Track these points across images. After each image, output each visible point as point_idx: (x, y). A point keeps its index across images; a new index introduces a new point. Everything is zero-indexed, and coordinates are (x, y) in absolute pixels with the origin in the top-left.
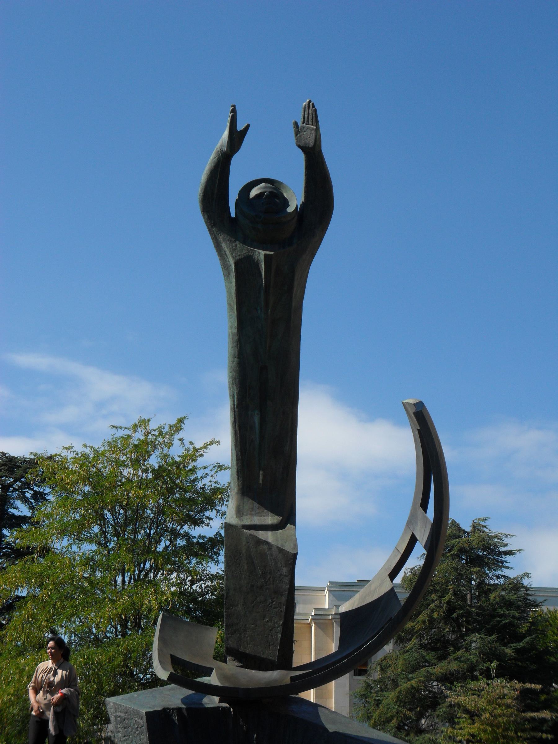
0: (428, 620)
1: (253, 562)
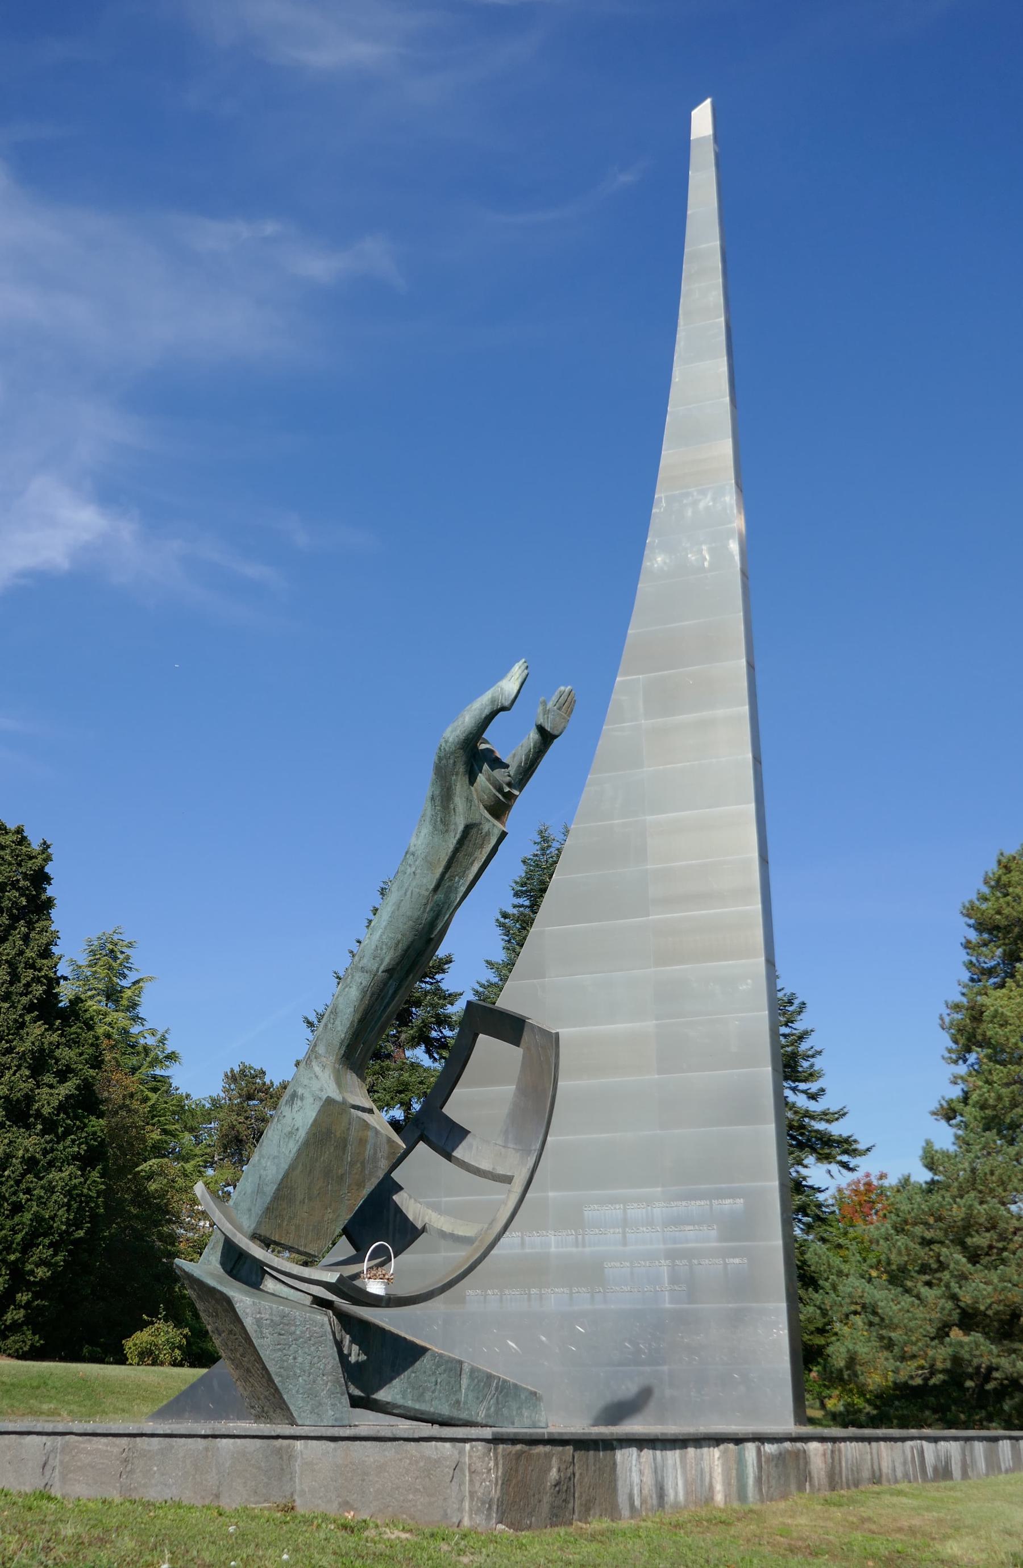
1: (346, 1146)
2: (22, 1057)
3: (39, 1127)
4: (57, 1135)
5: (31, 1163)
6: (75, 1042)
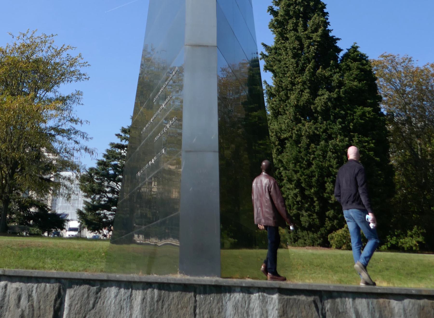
0: (299, 115)
2: (304, 83)
3: (320, 117)
4: (331, 121)
5: (314, 138)
6: (347, 70)
